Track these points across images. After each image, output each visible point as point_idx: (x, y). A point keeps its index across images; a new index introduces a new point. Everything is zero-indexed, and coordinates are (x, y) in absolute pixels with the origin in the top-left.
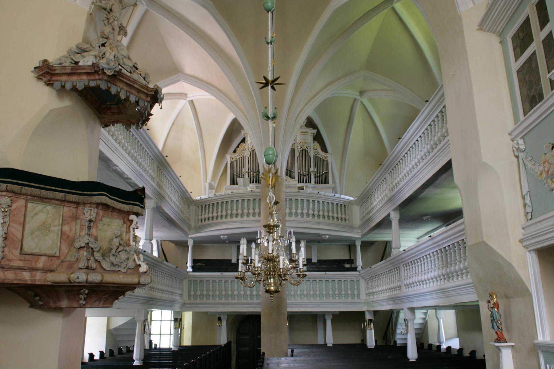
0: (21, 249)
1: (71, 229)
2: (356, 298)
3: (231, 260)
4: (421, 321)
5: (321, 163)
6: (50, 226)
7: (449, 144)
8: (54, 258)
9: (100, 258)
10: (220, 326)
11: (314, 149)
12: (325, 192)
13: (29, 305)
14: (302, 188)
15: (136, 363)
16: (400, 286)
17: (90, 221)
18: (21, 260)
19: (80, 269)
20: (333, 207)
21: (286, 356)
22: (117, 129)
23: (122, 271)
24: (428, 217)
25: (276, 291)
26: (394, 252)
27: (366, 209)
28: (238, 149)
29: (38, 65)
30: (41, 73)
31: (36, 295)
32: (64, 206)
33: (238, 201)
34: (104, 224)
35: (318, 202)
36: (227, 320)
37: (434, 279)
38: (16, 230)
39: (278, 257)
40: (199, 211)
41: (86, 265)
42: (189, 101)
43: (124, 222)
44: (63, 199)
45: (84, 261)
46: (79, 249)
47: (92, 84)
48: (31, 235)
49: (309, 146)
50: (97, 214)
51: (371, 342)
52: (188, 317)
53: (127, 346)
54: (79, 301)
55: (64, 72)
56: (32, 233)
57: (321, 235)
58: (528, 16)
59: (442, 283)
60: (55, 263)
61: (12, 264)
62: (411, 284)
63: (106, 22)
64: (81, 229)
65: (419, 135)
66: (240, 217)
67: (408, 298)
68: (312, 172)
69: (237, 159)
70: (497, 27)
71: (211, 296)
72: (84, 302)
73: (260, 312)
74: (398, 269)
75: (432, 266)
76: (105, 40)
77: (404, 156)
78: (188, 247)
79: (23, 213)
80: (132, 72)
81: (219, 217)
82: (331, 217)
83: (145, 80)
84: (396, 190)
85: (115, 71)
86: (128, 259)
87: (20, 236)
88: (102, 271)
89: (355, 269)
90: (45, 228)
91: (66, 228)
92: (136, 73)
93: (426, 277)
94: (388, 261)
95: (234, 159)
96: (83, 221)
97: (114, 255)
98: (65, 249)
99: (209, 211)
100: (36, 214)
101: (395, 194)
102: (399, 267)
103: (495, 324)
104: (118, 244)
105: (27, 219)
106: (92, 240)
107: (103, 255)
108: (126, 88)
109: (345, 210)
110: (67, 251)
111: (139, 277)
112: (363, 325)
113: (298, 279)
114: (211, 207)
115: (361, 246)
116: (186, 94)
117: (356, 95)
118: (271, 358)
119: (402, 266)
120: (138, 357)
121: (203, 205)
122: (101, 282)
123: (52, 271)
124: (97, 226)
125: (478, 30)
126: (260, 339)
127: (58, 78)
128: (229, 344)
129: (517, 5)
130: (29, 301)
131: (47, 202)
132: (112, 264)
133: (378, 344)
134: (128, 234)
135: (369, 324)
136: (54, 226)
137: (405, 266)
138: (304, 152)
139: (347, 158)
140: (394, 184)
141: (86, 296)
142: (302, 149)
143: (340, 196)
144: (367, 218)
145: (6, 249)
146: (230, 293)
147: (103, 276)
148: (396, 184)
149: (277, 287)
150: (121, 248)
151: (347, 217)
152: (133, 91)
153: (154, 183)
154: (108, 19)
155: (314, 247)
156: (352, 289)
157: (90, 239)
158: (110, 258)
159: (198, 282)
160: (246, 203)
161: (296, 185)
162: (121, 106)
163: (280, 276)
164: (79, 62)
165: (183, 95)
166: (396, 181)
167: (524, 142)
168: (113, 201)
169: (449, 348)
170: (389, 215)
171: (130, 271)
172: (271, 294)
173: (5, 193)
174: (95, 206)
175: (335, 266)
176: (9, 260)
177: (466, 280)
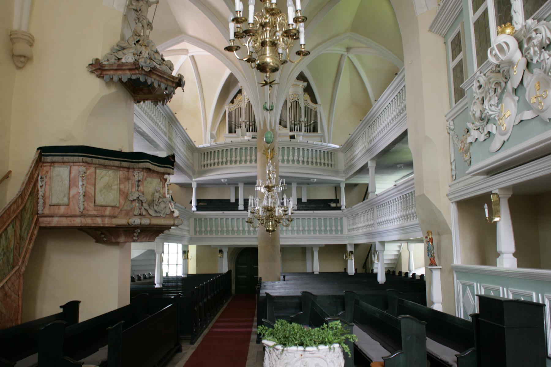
0: (95, 202)
1: (125, 187)
2: (339, 233)
3: (229, 200)
4: (396, 253)
5: (311, 114)
6: (112, 186)
7: (406, 117)
8: (116, 208)
9: (147, 208)
10: (221, 257)
11: (304, 100)
12: (313, 141)
13: (94, 240)
14: (292, 137)
15: (157, 286)
16: (374, 224)
17: (139, 181)
18: (95, 210)
19: (135, 215)
20: (321, 154)
21: (279, 280)
22: (147, 105)
23: (163, 216)
24: (401, 165)
25: (273, 231)
26: (370, 196)
27: (349, 157)
28: (235, 100)
29: (91, 62)
30: (94, 69)
31: (102, 234)
32: (120, 170)
33: (231, 149)
34: (148, 183)
35: (308, 150)
36: (228, 252)
37: (398, 219)
38: (91, 189)
39: (275, 208)
40: (201, 158)
41: (139, 213)
42: (190, 56)
43: (161, 180)
44: (120, 166)
45: (138, 210)
46: (132, 201)
47: (134, 77)
48: (100, 192)
49: (300, 97)
50: (143, 176)
51: (351, 270)
52: (193, 250)
53: (143, 274)
54: (133, 238)
55: (112, 68)
56: (101, 191)
57: (309, 179)
58: (460, 31)
59: (403, 222)
60: (117, 211)
61: (90, 213)
62: (381, 223)
63: (137, 21)
64: (132, 187)
65: (391, 100)
66: (238, 163)
67: (379, 233)
68: (303, 121)
69: (235, 109)
70: (442, 32)
71: (214, 232)
72: (136, 238)
73: (257, 245)
74: (372, 209)
75: (396, 208)
76: (138, 38)
77: (380, 115)
78: (192, 188)
79: (94, 177)
80: (161, 64)
81: (220, 163)
82: (318, 163)
83: (170, 70)
84: (373, 144)
85: (151, 68)
86: (165, 207)
87: (93, 194)
88: (149, 217)
89: (339, 208)
90: (108, 187)
91: (122, 187)
92: (163, 65)
93: (386, 219)
94: (365, 203)
95: (232, 110)
96: (134, 181)
97: (156, 205)
98: (122, 202)
99: (211, 158)
100: (102, 178)
101: (372, 147)
102: (373, 208)
103: (429, 253)
104: (158, 197)
105: (97, 181)
106: (141, 194)
107: (149, 205)
108: (158, 78)
109: (331, 156)
110: (123, 202)
111: (174, 220)
112: (344, 256)
113: (288, 222)
114: (213, 154)
115: (345, 188)
116: (188, 50)
117: (342, 51)
118: (267, 282)
119: (376, 208)
120: (159, 282)
121: (206, 153)
122: (150, 225)
123: (115, 217)
124: (143, 184)
125: (429, 31)
126: (257, 268)
127: (107, 73)
128: (229, 272)
129: (454, 20)
130: (95, 238)
131: (108, 168)
132: (156, 211)
133: (358, 272)
134: (164, 189)
135: (350, 255)
136: (114, 185)
137: (377, 207)
138: (296, 103)
139: (334, 110)
140: (371, 138)
141: (138, 234)
142: (293, 101)
143: (327, 145)
144: (350, 164)
145: (85, 203)
146: (230, 229)
147: (150, 220)
148: (373, 138)
149: (274, 227)
150: (161, 200)
151: (333, 163)
152: (163, 80)
153: (166, 137)
154: (138, 18)
155: (304, 188)
156: (336, 226)
157: (140, 194)
158: (155, 207)
159: (203, 219)
160: (244, 150)
161: (288, 133)
162: (151, 89)
163: (276, 221)
164: (122, 59)
165: (186, 51)
166: (373, 136)
167: (454, 123)
168: (154, 166)
169: (414, 275)
170: (367, 164)
171: (168, 216)
172: (270, 232)
173: (81, 164)
174: (141, 170)
175: (323, 205)
176: (87, 210)
177: (416, 221)
